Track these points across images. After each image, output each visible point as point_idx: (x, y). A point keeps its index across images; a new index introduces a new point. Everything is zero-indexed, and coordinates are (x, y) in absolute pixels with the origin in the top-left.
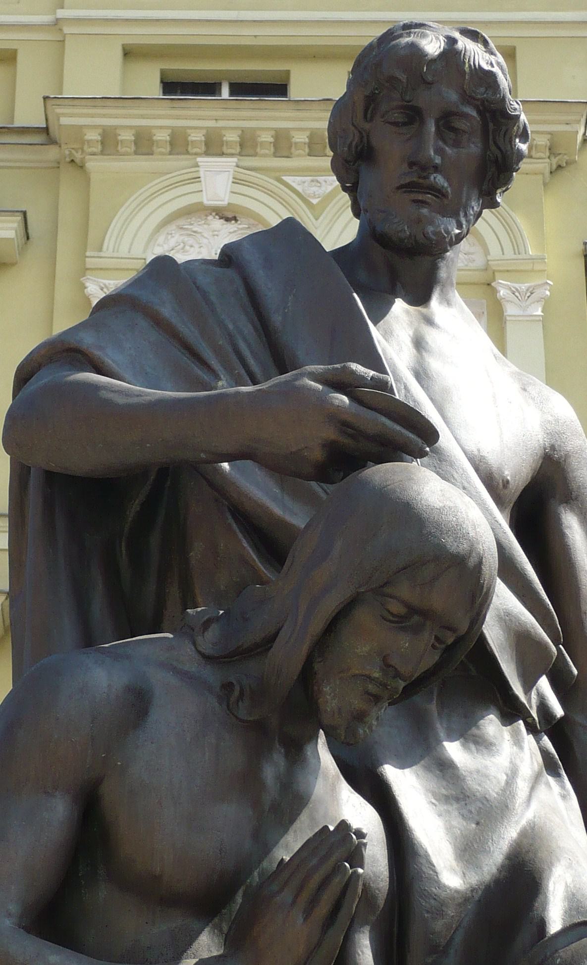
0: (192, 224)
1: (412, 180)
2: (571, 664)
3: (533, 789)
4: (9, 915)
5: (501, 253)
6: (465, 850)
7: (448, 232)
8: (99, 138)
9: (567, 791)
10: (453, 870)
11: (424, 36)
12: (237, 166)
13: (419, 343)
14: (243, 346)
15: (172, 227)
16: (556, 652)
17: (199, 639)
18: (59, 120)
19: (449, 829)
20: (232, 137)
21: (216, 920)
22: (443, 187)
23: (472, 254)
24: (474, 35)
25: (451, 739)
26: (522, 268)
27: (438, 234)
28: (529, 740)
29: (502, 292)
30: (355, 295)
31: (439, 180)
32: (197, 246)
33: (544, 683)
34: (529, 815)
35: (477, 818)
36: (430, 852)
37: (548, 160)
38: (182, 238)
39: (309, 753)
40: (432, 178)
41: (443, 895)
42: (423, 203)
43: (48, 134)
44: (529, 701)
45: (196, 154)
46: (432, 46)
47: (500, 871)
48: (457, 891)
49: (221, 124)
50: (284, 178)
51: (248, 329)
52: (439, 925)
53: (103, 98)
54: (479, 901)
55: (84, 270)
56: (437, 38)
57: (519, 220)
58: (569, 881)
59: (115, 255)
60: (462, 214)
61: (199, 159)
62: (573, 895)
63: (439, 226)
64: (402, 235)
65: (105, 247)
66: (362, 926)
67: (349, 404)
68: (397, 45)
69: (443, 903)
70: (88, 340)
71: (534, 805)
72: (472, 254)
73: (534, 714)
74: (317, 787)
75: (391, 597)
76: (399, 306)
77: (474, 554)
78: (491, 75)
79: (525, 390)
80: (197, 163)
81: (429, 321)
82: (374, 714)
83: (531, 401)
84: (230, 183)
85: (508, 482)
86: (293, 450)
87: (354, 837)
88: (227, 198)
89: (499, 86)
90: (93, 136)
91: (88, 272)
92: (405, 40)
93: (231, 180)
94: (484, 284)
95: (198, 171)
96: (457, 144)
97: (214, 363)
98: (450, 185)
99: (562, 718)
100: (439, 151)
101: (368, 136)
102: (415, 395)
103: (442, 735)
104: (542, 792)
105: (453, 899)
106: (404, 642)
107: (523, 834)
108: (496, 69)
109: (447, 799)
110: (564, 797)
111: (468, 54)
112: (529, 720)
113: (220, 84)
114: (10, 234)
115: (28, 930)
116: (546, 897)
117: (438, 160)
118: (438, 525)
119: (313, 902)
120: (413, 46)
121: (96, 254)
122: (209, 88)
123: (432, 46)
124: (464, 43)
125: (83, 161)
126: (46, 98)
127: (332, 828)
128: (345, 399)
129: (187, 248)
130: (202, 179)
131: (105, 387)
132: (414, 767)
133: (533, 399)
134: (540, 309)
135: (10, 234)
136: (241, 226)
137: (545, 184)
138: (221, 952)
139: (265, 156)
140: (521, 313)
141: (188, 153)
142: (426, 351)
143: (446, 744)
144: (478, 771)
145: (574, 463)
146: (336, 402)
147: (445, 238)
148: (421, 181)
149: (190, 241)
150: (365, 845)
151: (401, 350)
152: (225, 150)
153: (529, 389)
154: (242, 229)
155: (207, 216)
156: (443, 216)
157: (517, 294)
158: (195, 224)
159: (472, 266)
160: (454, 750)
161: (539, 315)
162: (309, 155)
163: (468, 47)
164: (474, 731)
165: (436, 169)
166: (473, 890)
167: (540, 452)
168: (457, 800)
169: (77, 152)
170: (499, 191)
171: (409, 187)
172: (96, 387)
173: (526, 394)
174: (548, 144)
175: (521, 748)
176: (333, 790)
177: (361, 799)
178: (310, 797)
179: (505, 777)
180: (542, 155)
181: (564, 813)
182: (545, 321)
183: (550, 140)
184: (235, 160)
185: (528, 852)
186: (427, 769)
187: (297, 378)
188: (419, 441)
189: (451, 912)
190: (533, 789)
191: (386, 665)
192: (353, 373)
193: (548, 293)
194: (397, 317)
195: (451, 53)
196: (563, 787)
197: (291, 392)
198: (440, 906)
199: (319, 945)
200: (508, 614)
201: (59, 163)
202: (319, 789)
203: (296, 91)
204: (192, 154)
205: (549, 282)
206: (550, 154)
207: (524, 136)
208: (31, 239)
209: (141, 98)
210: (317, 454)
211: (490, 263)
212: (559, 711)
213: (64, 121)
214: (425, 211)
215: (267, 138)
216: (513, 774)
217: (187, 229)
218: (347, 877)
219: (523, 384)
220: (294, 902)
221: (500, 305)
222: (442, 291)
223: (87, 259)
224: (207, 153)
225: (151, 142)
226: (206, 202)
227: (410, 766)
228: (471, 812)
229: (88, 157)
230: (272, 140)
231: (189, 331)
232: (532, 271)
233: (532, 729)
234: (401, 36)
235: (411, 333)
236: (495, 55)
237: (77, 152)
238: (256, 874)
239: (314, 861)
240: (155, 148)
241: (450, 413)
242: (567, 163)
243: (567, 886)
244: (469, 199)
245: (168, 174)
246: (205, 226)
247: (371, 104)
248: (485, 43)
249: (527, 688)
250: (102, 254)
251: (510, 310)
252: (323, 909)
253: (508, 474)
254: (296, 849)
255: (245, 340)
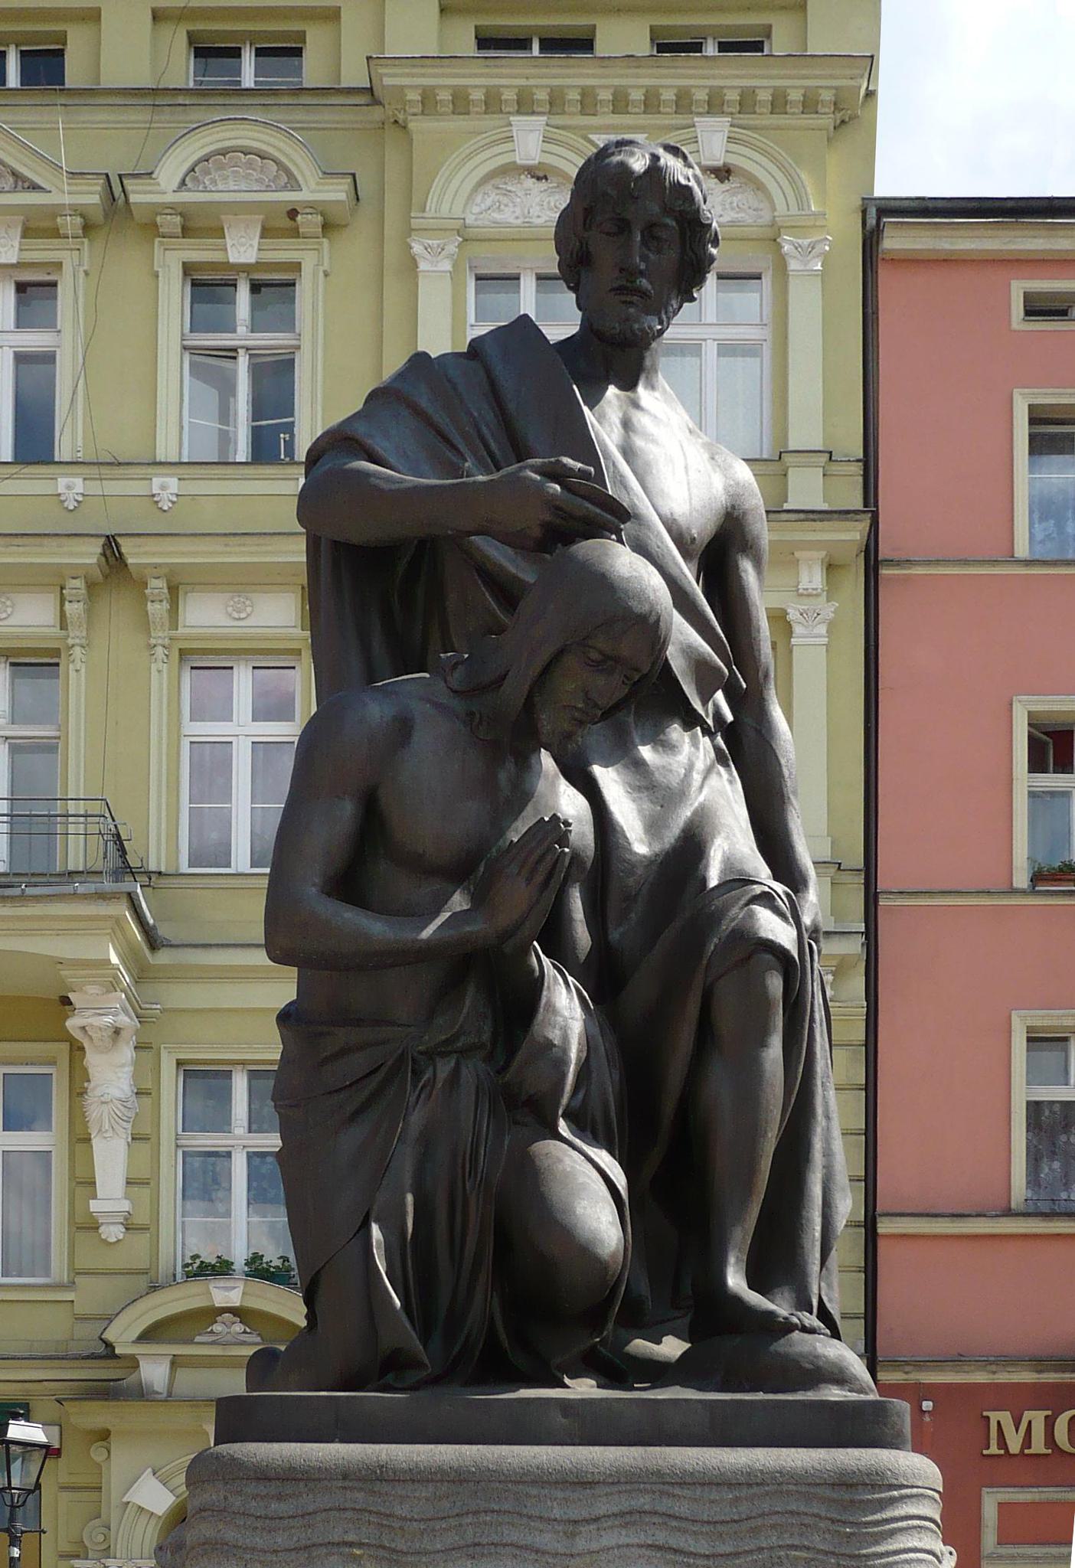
0: (506, 183)
1: (622, 283)
2: (741, 680)
3: (705, 779)
4: (314, 885)
5: (786, 209)
6: (651, 826)
7: (650, 328)
8: (420, 98)
9: (734, 777)
10: (641, 841)
11: (632, 154)
12: (547, 125)
13: (627, 424)
14: (485, 430)
15: (488, 187)
16: (728, 674)
17: (449, 678)
18: (382, 80)
19: (640, 811)
20: (542, 95)
21: (465, 884)
22: (647, 290)
23: (761, 210)
24: (674, 151)
25: (644, 744)
26: (804, 224)
27: (642, 330)
28: (705, 742)
29: (786, 248)
30: (575, 387)
31: (644, 283)
32: (511, 205)
33: (719, 696)
34: (701, 798)
35: (662, 802)
36: (625, 828)
37: (832, 116)
38: (498, 197)
39: (533, 761)
40: (638, 281)
41: (634, 859)
42: (631, 303)
43: (372, 95)
44: (706, 711)
45: (509, 113)
46: (638, 164)
47: (677, 841)
48: (645, 856)
49: (532, 82)
50: (590, 136)
51: (490, 416)
52: (631, 881)
53: (422, 57)
54: (662, 862)
55: (409, 231)
56: (644, 156)
57: (803, 176)
58: (726, 848)
59: (438, 215)
60: (663, 312)
61: (511, 118)
62: (728, 859)
63: (643, 323)
64: (613, 331)
65: (428, 208)
66: (575, 882)
67: (561, 492)
68: (608, 164)
69: (634, 866)
70: (361, 430)
71: (705, 791)
72: (761, 210)
73: (710, 721)
74: (539, 786)
75: (591, 647)
76: (612, 391)
77: (653, 613)
78: (688, 189)
79: (713, 459)
80: (510, 122)
81: (636, 405)
82: (580, 732)
83: (718, 469)
84: (540, 142)
85: (694, 538)
86: (519, 529)
87: (562, 826)
88: (537, 158)
89: (693, 199)
90: (413, 96)
91: (413, 233)
92: (616, 159)
93: (541, 138)
94: (770, 240)
95: (511, 130)
96: (659, 252)
97: (462, 447)
98: (653, 288)
99: (731, 723)
100: (644, 258)
101: (587, 244)
102: (621, 470)
103: (637, 740)
104: (713, 780)
105: (641, 862)
106: (601, 681)
107: (695, 813)
108: (692, 183)
109: (639, 789)
110: (731, 782)
111: (669, 170)
112: (705, 726)
113: (531, 39)
114: (342, 196)
115: (329, 895)
116: (708, 861)
117: (643, 266)
118: (626, 592)
119: (534, 871)
120: (622, 165)
121: (421, 215)
122: (521, 43)
123: (638, 164)
124: (667, 160)
125: (405, 121)
126: (369, 58)
127: (547, 819)
128: (558, 487)
129: (502, 207)
130: (515, 138)
131: (375, 475)
132: (616, 766)
133: (719, 466)
134: (820, 264)
135: (342, 196)
136: (551, 185)
137: (829, 140)
138: (469, 907)
139: (574, 114)
140: (802, 268)
141: (501, 112)
142: (633, 431)
143: (639, 747)
144: (664, 767)
145: (750, 518)
146: (551, 491)
147: (648, 333)
148: (629, 284)
149: (505, 200)
150: (570, 831)
151: (612, 431)
152: (536, 109)
153: (717, 457)
154: (552, 188)
155: (520, 175)
156: (647, 315)
157: (799, 249)
158: (510, 184)
159: (760, 222)
160: (646, 752)
161: (819, 270)
162: (613, 113)
163: (669, 164)
164: (662, 737)
165: (642, 273)
166: (657, 855)
167: (723, 512)
168: (647, 788)
169: (400, 112)
170: (694, 290)
171: (620, 290)
172: (366, 475)
173: (713, 462)
174: (833, 98)
175: (698, 749)
176: (553, 785)
177: (575, 791)
178: (533, 794)
179: (684, 771)
180: (827, 110)
181: (730, 794)
182: (824, 274)
183: (835, 95)
184: (545, 118)
185: (698, 827)
186: (626, 766)
187: (521, 469)
188: (616, 521)
189: (640, 871)
190: (705, 779)
191: (587, 698)
192: (565, 465)
193: (827, 248)
194: (610, 402)
195: (655, 169)
196: (731, 774)
197: (516, 479)
198: (632, 864)
199: (538, 901)
200: (690, 646)
201: (383, 124)
202: (541, 786)
203: (601, 48)
204: (506, 113)
205: (829, 237)
206: (835, 109)
207: (715, 242)
208: (361, 201)
209: (456, 57)
210: (536, 532)
211: (777, 219)
212: (729, 717)
213: (387, 81)
214: (632, 310)
215: (574, 95)
216: (690, 768)
217: (502, 188)
218: (557, 854)
219: (713, 454)
220: (519, 874)
221: (784, 259)
222: (647, 378)
223: (412, 220)
224: (519, 112)
225: (467, 101)
226: (519, 162)
227: (612, 765)
228: (657, 798)
229: (410, 118)
230: (579, 98)
231: (441, 419)
232: (815, 226)
233: (707, 732)
234: (613, 154)
235: (621, 415)
236: (693, 168)
237: (400, 112)
238: (494, 850)
239: (533, 844)
240: (471, 107)
241: (649, 480)
242: (850, 118)
243: (724, 852)
244: (669, 299)
245: (483, 133)
246: (519, 185)
247: (588, 212)
248: (685, 158)
249: (705, 703)
250: (426, 215)
251: (793, 265)
252: (539, 878)
253: (695, 532)
254: (523, 832)
255: (487, 426)
